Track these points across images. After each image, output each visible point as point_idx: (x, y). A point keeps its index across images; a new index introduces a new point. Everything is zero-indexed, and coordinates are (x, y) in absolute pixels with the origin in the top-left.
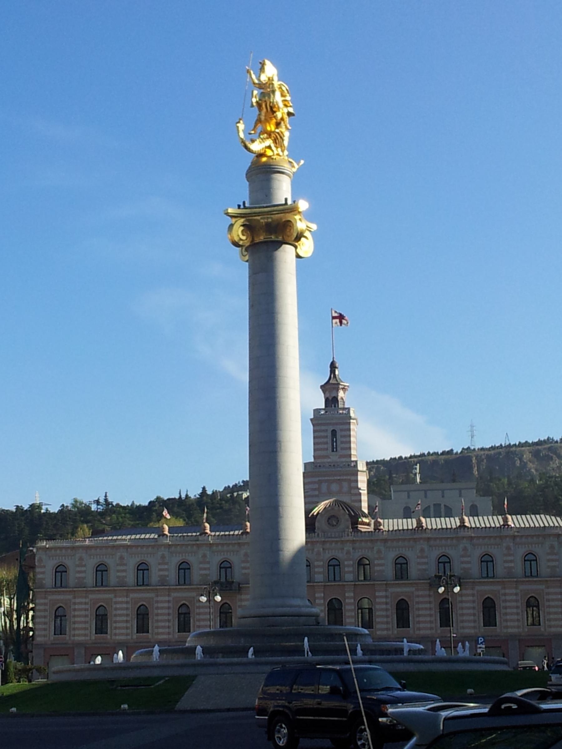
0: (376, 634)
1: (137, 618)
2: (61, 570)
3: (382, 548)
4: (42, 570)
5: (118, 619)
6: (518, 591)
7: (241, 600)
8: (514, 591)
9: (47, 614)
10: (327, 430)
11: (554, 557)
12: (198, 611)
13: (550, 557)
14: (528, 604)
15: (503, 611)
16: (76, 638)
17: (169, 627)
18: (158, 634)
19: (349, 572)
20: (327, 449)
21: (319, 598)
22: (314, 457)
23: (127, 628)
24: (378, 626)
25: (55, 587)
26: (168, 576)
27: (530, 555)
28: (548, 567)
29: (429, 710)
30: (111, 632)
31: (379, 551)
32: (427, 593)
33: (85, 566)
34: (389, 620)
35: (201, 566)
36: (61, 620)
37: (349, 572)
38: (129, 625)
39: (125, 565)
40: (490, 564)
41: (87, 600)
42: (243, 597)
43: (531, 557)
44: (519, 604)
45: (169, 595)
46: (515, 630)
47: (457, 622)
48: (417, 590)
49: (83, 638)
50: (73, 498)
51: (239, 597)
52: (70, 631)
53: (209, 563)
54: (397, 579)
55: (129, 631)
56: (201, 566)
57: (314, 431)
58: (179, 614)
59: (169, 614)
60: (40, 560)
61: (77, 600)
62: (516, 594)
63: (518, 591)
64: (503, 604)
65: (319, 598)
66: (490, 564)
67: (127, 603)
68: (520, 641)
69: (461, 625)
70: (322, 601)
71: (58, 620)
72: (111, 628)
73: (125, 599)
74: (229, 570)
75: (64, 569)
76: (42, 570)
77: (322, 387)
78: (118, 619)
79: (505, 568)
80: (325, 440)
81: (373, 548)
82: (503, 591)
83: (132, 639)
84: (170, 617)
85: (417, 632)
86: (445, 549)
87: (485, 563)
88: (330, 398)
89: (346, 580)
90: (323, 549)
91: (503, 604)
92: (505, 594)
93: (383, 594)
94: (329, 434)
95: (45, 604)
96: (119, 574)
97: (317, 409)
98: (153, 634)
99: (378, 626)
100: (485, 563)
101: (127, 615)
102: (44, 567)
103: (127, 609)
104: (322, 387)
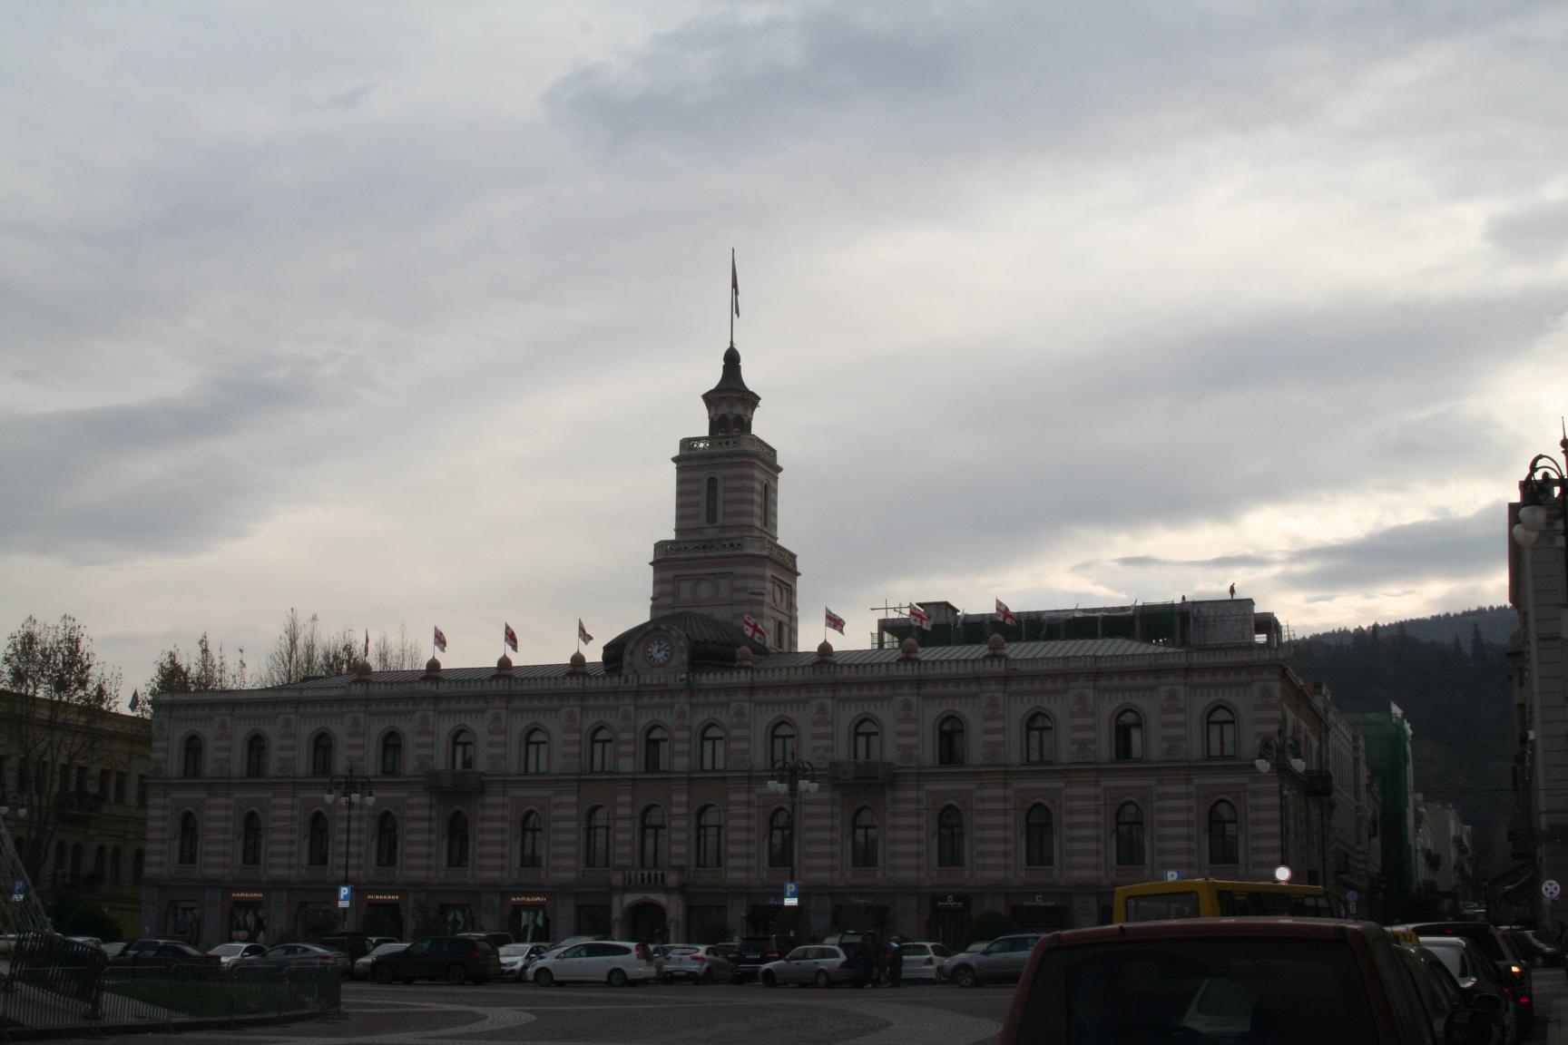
3: (503, 712)
5: (1076, 832)
6: (753, 797)
11: (823, 730)
16: (1076, 873)
22: (678, 531)
25: (186, 776)
28: (815, 749)
34: (753, 849)
36: (656, 836)
38: (1010, 847)
43: (1221, 715)
49: (497, 874)
59: (832, 829)
62: (1005, 799)
74: (1228, 729)
75: (874, 729)
78: (1076, 832)
80: (730, 496)
81: (728, 705)
84: (753, 836)
93: (743, 797)
94: (703, 487)
95: (503, 806)
103: (1189, 810)
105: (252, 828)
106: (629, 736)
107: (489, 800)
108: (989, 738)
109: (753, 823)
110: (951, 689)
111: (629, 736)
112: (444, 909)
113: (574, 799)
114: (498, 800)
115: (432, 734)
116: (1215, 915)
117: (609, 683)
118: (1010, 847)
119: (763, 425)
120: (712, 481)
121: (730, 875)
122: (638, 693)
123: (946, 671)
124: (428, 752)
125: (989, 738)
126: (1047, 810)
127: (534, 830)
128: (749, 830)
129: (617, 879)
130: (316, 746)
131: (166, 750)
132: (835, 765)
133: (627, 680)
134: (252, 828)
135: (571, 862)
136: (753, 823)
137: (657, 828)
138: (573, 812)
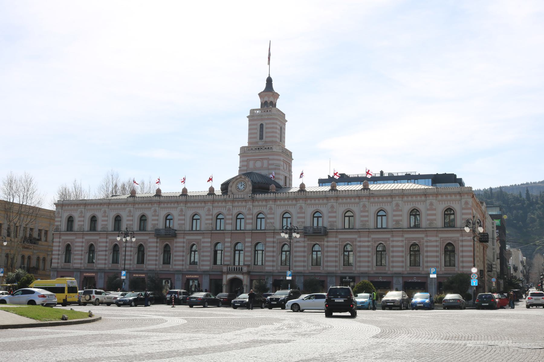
7: (176, 242)
8: (105, 240)
10: (257, 124)
12: (438, 249)
14: (446, 251)
15: (425, 254)
17: (183, 261)
20: (256, 138)
23: (304, 261)
26: (336, 222)
27: (349, 212)
29: (162, 321)
31: (271, 208)
32: (155, 240)
33: (335, 212)
35: (464, 211)
38: (306, 259)
41: (370, 239)
42: (330, 239)
44: (275, 249)
45: (368, 237)
46: (366, 269)
47: (423, 262)
48: (204, 238)
50: (19, 174)
51: (175, 240)
52: (389, 263)
53: (304, 213)
54: (91, 230)
55: (337, 264)
57: (250, 125)
58: (377, 251)
61: (395, 239)
63: (84, 240)
64: (425, 249)
67: (82, 242)
68: (105, 272)
70: (250, 244)
72: (423, 262)
73: (366, 239)
77: (259, 94)
83: (441, 270)
88: (269, 102)
90: (233, 207)
93: (272, 240)
94: (258, 127)
97: (254, 110)
98: (459, 267)
101: (336, 252)
104: (259, 94)
107: (179, 240)
108: (362, 219)
114: (182, 240)
119: (280, 105)
120: (262, 125)
121: (267, 268)
125: (362, 219)
127: (195, 251)
133: (229, 196)
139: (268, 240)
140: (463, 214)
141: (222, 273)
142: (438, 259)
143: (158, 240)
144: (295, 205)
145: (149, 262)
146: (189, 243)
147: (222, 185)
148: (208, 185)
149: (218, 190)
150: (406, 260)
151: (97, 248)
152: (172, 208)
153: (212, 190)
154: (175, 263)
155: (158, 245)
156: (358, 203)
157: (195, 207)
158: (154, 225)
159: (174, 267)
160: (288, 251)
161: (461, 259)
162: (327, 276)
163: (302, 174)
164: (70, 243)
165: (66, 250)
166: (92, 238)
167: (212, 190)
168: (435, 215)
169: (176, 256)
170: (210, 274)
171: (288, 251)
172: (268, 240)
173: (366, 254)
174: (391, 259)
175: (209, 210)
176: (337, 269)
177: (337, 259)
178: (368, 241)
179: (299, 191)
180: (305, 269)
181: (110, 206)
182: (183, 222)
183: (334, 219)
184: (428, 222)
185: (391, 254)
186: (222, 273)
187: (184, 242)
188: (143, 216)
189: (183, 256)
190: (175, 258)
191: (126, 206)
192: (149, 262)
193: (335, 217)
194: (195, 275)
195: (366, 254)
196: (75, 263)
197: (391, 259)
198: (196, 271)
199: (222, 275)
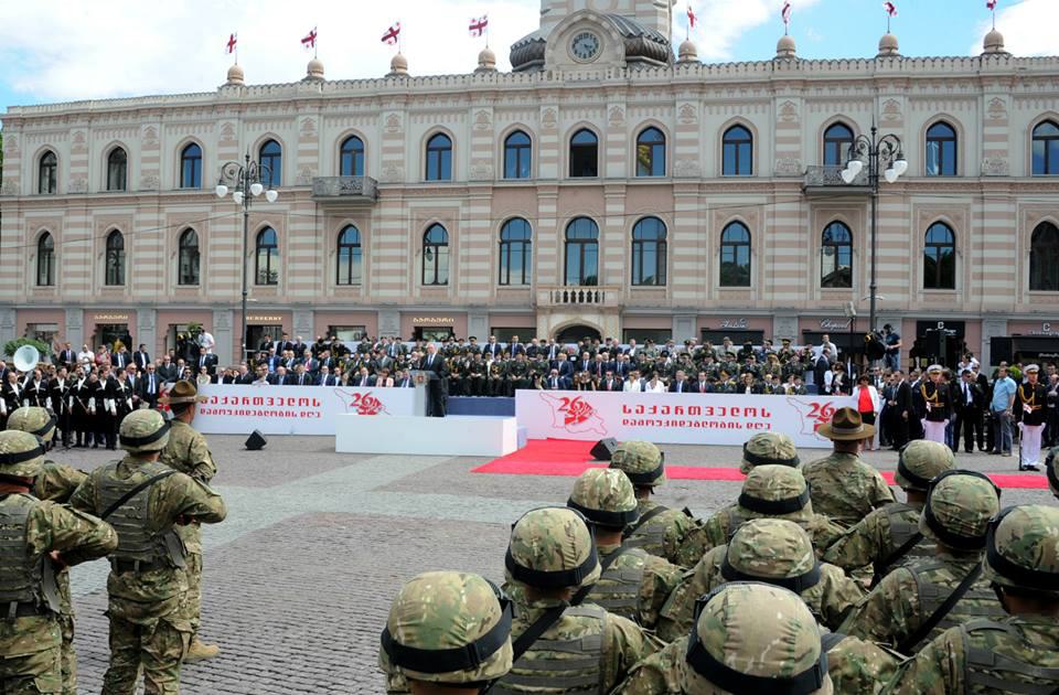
0: (671, 297)
1: (338, 254)
2: (519, 143)
4: (15, 161)
6: (22, 221)
7: (379, 218)
9: (406, 239)
13: (303, 146)
18: (378, 286)
19: (616, 161)
21: (548, 216)
24: (678, 280)
30: (968, 284)
32: (795, 207)
37: (551, 162)
39: (402, 136)
40: (948, 145)
47: (760, 274)
51: (375, 212)
56: (781, 133)
59: (316, 246)
60: (12, 143)
65: (548, 216)
66: (948, 145)
69: (803, 282)
71: (264, 253)
76: (15, 161)
79: (777, 155)
82: (464, 211)
84: (320, 253)
85: (373, 293)
86: (50, 140)
87: (834, 144)
89: (542, 177)
91: (463, 238)
92: (468, 218)
96: (781, 148)
99: (678, 280)
100: (733, 146)
102: (19, 155)
105: (189, 249)
106: (553, 139)
107: (385, 211)
108: (387, 157)
109: (162, 242)
110: (352, 108)
111: (553, 139)
112: (332, 331)
113: (487, 210)
114: (397, 211)
115: (316, 140)
116: (799, 345)
117: (527, 80)
118: (405, 266)
121: (677, 295)
122: (562, 92)
123: (443, 85)
124: (82, 169)
125: (387, 157)
126: (948, 227)
127: (437, 246)
128: (158, 248)
129: (543, 298)
130: (42, 166)
131: (19, 167)
132: (319, 181)
133: (550, 75)
134: (189, 249)
135: (485, 280)
136: (162, 242)
137: (351, 246)
138: (487, 223)
139: (678, 207)
140: (778, 140)
141: (535, 311)
142: (803, 267)
143: (321, 213)
144: (293, 118)
145: (66, 280)
146: (101, 227)
147: (515, 48)
148: (476, 45)
149: (504, 65)
150: (412, 267)
151: (129, 243)
152: (451, 111)
153: (486, 61)
154: (211, 280)
155: (321, 226)
156: (466, 111)
157: (268, 119)
158: (306, 169)
159: (290, 293)
160: (743, 244)
161: (768, 267)
162: (772, 317)
163: (232, 43)
164: (116, 226)
165: (109, 249)
166: (114, 214)
167: (486, 61)
168: (401, 150)
169: (138, 261)
170: (490, 314)
171: (743, 244)
172: (543, 209)
173: (397, 252)
174: (374, 266)
175: (483, 119)
176: (319, 293)
177: (405, 266)
178: (403, 219)
179: (477, 70)
180: (161, 292)
181: (165, 117)
182: (989, 130)
183: (82, 169)
184: (386, 169)
185: (374, 253)
186: (535, 311)
187: (86, 225)
188: (49, 153)
189: (316, 260)
190: (136, 268)
191: (139, 120)
192: (66, 280)
193: (315, 153)
194: (442, 314)
195: (397, 252)
196: (66, 287)
197: (374, 266)
198: (449, 306)
199: (534, 316)
